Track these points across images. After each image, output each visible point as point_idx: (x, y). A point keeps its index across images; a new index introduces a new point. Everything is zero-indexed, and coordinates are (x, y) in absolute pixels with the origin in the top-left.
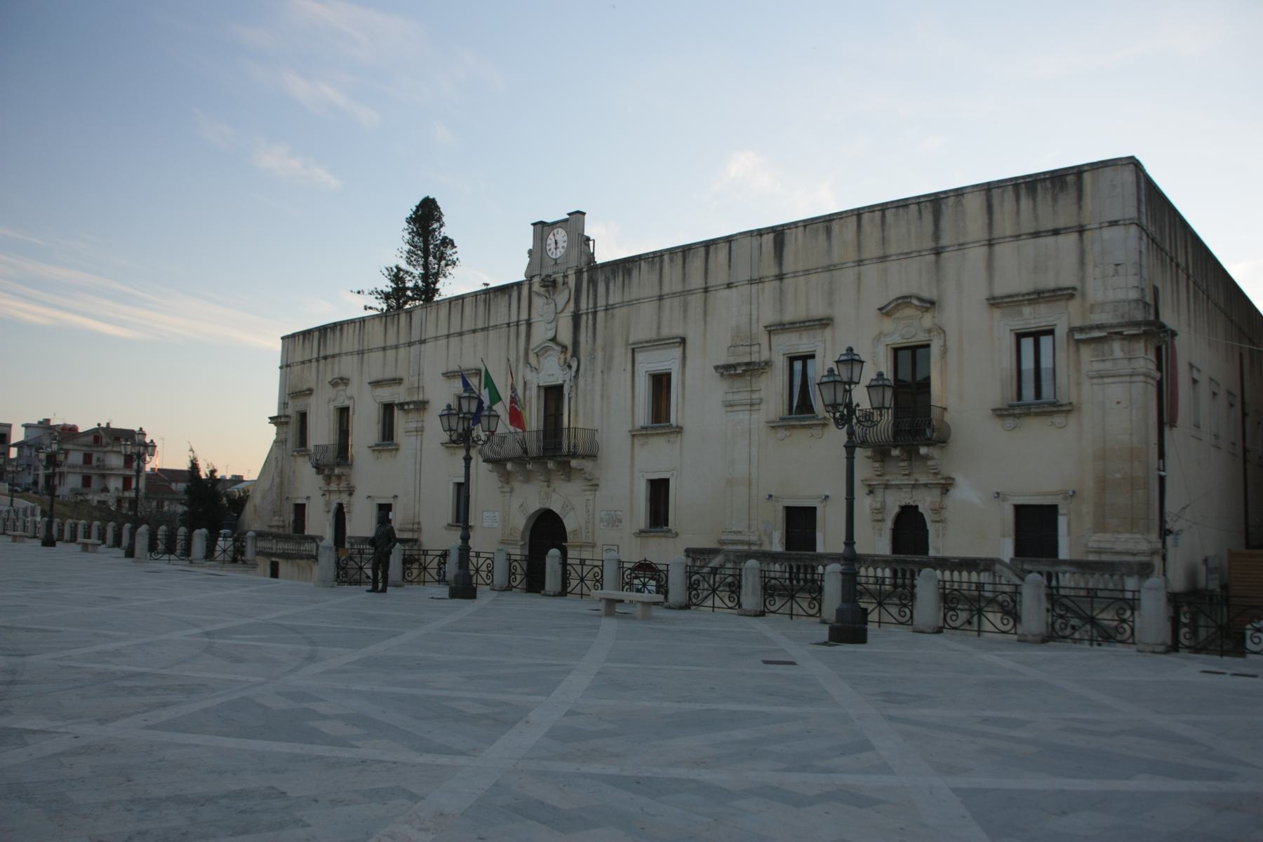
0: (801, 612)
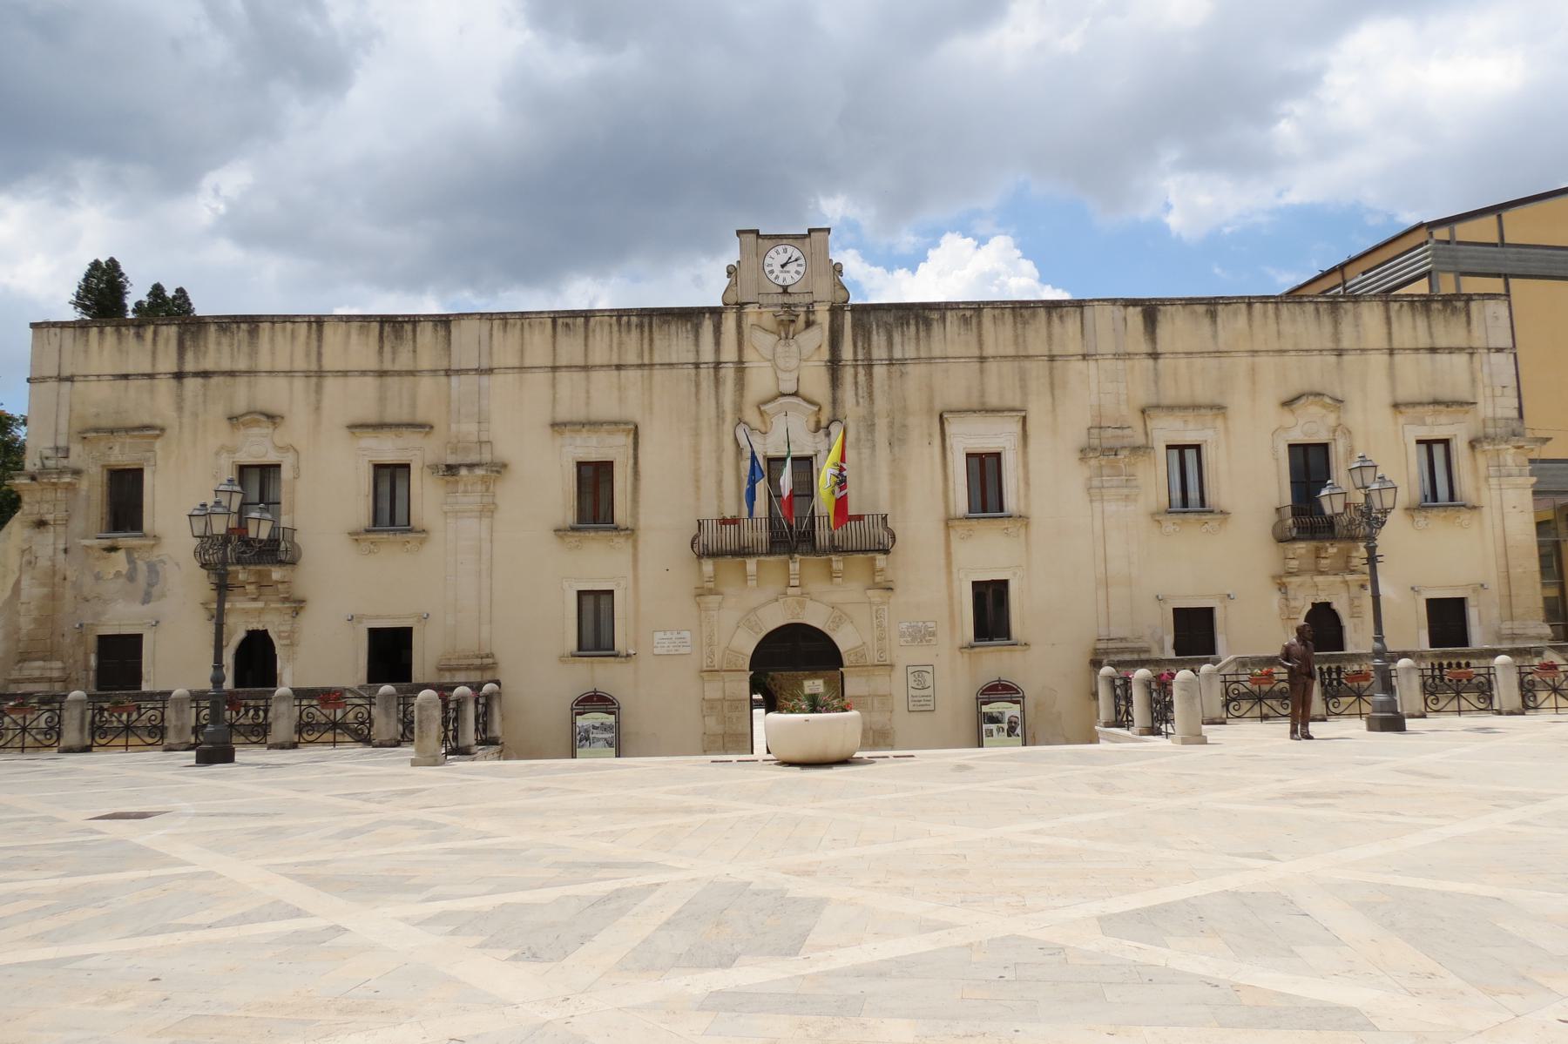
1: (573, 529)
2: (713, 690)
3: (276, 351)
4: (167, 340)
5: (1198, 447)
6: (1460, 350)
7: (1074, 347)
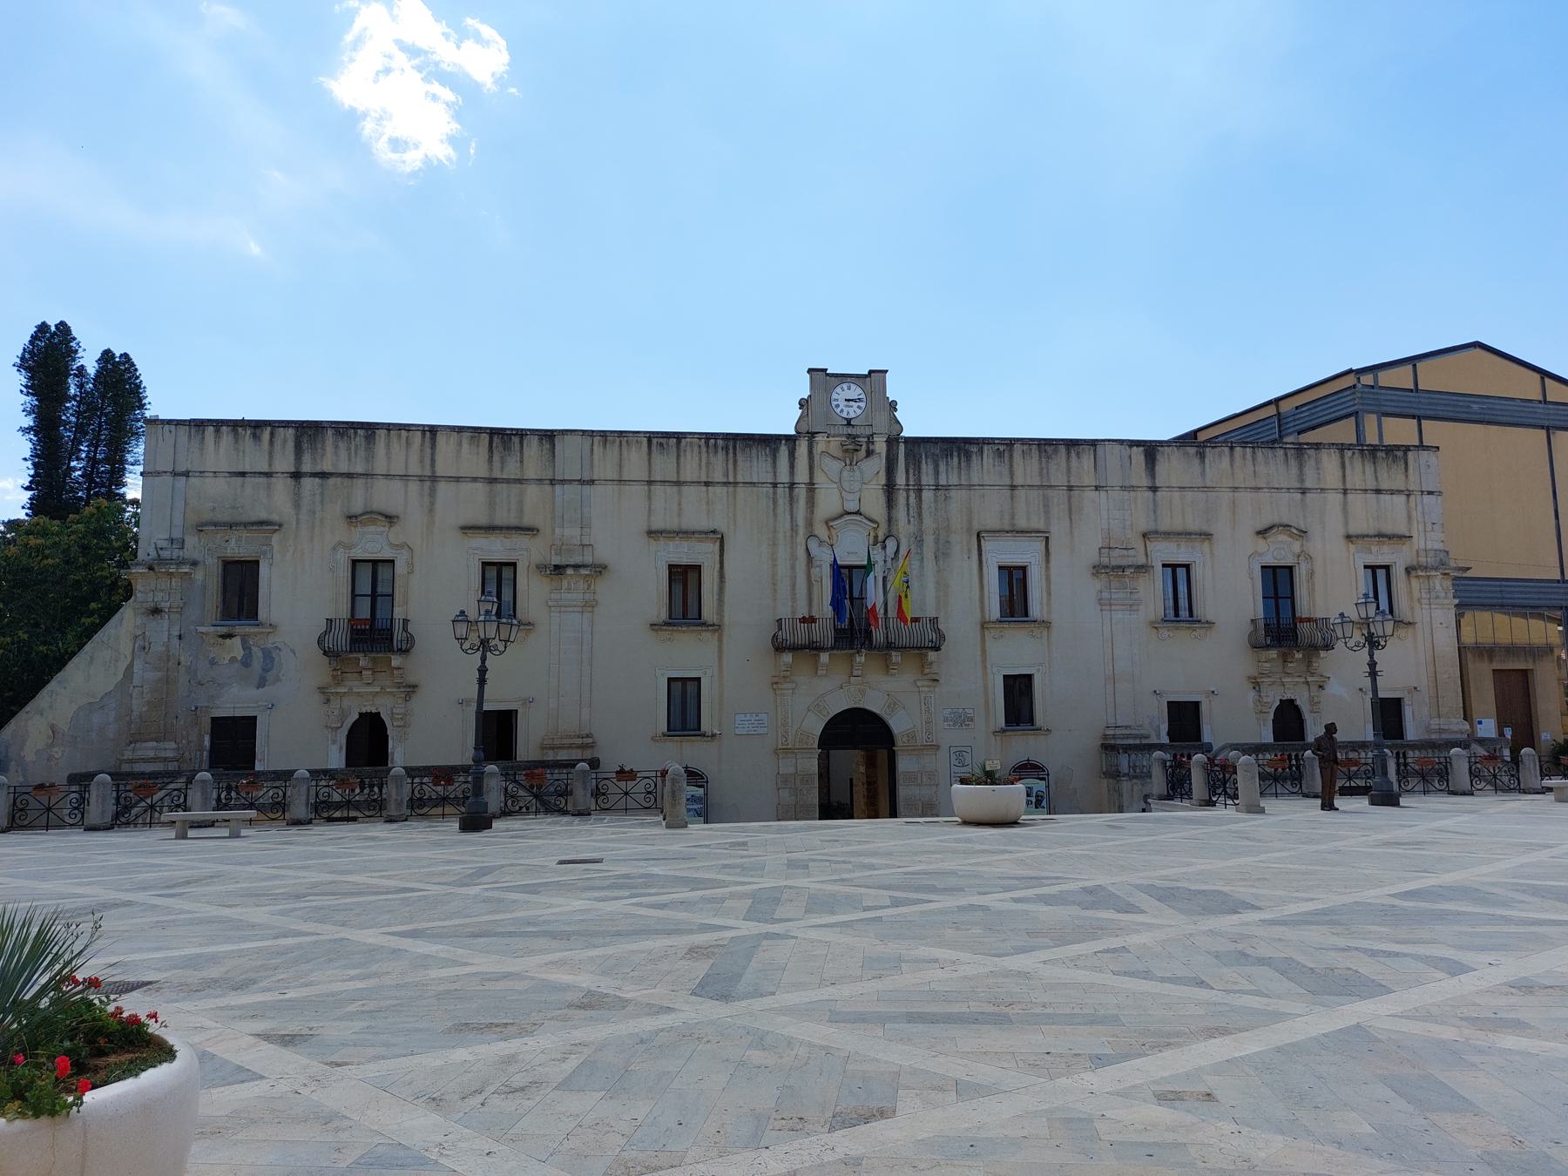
0: (636, 805)
1: (666, 624)
2: (787, 767)
3: (389, 457)
4: (285, 441)
5: (1187, 567)
6: (1400, 492)
7: (1089, 479)
